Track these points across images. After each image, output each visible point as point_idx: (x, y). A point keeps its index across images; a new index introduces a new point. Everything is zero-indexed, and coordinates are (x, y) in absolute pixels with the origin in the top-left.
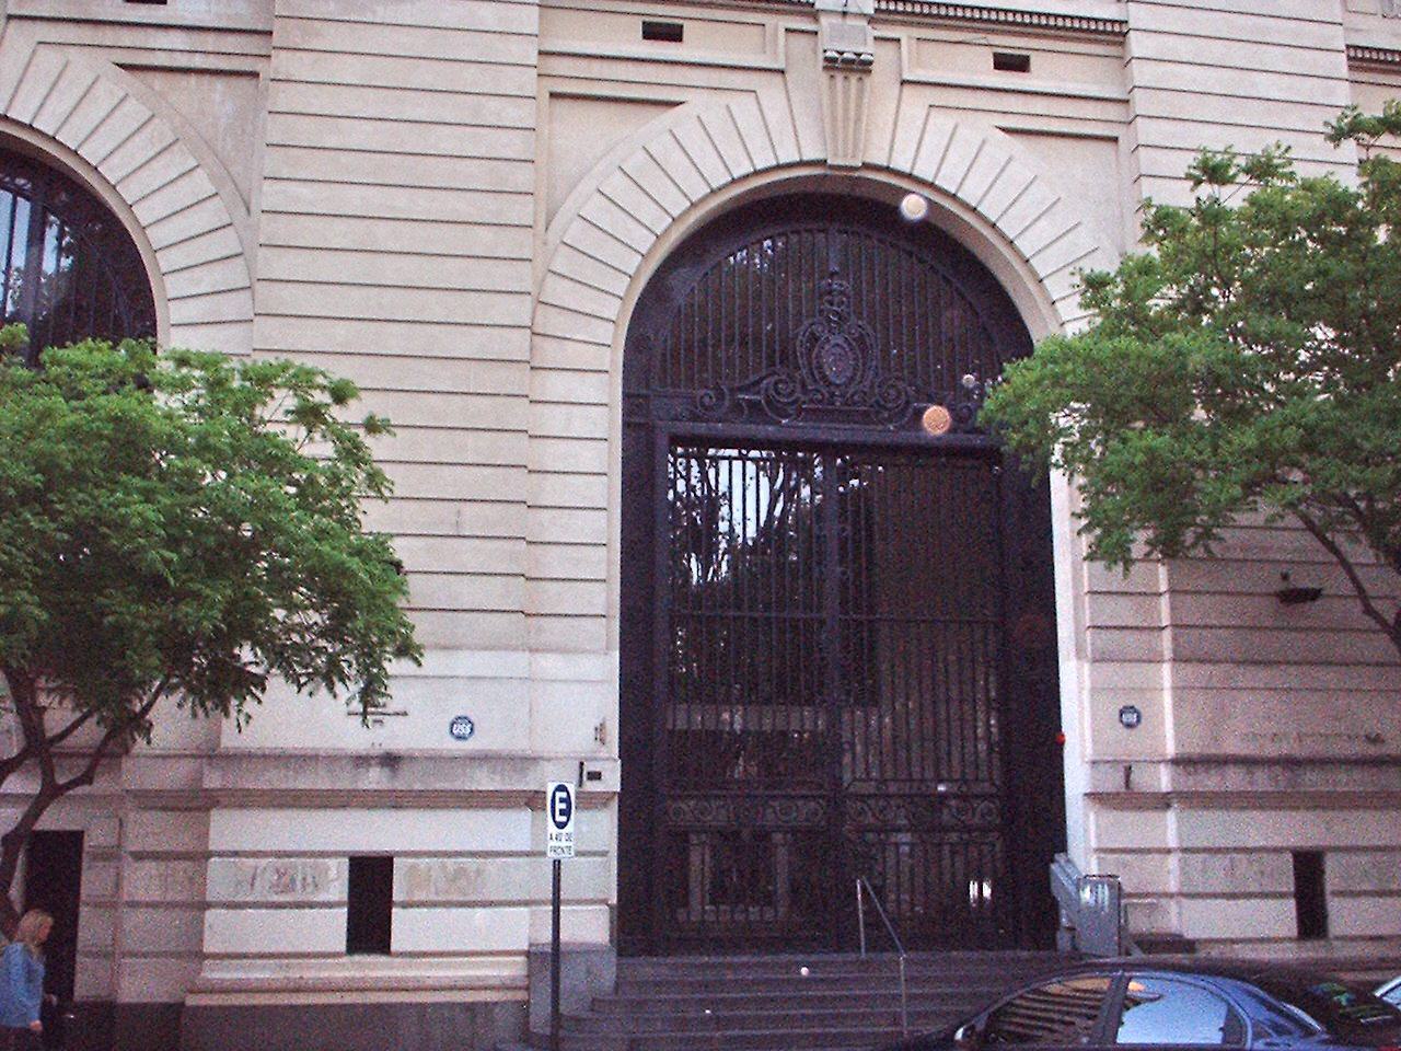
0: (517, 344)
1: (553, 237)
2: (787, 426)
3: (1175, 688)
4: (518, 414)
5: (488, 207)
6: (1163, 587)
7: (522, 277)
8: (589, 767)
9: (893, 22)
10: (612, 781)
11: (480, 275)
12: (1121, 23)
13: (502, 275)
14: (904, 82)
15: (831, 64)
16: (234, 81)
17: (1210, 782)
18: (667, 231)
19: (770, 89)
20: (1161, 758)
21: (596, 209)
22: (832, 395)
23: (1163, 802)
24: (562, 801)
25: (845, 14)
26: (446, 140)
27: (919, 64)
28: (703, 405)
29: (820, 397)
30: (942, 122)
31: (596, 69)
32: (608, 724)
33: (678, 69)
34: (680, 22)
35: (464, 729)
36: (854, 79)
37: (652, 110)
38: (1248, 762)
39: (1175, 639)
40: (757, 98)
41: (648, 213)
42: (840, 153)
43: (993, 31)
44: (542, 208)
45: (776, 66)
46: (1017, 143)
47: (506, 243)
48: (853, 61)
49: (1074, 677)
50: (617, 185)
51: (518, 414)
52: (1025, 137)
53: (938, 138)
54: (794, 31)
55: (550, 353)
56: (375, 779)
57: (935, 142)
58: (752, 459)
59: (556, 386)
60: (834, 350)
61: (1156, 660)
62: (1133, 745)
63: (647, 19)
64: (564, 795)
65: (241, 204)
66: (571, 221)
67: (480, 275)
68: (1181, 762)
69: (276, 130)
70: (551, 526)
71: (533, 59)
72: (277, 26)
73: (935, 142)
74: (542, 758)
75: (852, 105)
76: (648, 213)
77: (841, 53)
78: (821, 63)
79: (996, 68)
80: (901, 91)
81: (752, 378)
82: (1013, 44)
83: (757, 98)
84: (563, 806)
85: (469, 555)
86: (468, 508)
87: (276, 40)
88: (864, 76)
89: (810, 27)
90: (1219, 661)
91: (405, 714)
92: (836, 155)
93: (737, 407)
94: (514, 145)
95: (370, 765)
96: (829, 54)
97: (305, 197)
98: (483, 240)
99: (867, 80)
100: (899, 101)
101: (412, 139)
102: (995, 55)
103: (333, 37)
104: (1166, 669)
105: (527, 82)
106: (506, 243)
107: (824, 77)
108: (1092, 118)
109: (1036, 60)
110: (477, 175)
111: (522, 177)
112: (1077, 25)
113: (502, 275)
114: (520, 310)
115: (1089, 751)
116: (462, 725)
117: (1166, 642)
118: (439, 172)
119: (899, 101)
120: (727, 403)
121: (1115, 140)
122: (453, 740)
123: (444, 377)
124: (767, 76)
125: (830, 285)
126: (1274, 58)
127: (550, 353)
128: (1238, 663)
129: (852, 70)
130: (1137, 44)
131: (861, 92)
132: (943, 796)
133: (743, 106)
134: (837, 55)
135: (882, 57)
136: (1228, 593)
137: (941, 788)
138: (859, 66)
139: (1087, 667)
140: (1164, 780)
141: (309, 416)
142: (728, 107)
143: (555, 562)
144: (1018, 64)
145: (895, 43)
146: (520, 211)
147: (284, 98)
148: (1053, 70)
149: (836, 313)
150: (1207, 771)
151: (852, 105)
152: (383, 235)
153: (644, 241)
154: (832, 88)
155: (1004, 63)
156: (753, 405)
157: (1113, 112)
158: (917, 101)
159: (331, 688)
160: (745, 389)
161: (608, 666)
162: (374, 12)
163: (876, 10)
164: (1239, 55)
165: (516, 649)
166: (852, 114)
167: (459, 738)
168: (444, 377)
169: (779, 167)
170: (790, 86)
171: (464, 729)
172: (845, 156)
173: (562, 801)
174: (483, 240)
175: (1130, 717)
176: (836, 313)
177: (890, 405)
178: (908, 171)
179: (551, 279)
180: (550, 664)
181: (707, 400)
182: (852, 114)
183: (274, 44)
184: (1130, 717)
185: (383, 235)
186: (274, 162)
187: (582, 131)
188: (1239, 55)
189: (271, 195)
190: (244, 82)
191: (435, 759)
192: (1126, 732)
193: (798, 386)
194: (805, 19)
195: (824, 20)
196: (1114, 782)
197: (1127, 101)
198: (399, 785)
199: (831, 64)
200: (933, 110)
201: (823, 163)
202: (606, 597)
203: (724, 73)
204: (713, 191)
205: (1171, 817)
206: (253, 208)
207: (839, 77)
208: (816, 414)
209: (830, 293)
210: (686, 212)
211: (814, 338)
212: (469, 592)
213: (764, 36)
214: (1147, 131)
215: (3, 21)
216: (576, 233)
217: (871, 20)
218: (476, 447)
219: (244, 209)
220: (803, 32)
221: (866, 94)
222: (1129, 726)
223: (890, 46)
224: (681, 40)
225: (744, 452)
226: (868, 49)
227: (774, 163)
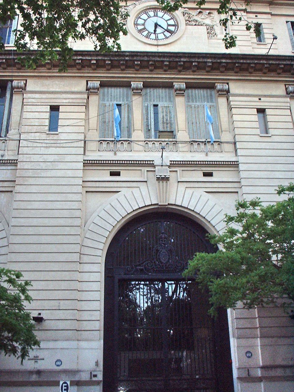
0: (76, 257)
1: (86, 228)
2: (151, 275)
3: (261, 346)
4: (78, 276)
5: (69, 222)
6: (257, 316)
7: (78, 239)
8: (94, 373)
9: (176, 167)
10: (100, 377)
11: (65, 239)
12: (237, 162)
13: (72, 239)
14: (178, 182)
15: (158, 179)
16: (6, 193)
17: (272, 373)
18: (116, 225)
19: (143, 186)
20: (258, 366)
21: (97, 220)
22: (163, 266)
23: (260, 380)
24: (65, 386)
25: (162, 166)
26: (58, 205)
27: (183, 177)
28: (127, 270)
29: (159, 266)
30: (189, 191)
31: (98, 184)
32: (99, 362)
33: (105, 183)
34: (211, 171)
35: (59, 363)
36: (165, 182)
37: (112, 193)
38: (284, 367)
39: (260, 331)
40: (140, 189)
41: (111, 221)
42: (165, 201)
43: (203, 167)
44: (84, 222)
45: (145, 180)
46: (210, 195)
47: (73, 231)
48: (164, 178)
49: (233, 342)
50: (103, 214)
51: (78, 276)
52: (210, 194)
53: (189, 196)
54: (149, 171)
55: (85, 259)
56: (34, 378)
57: (187, 197)
58: (142, 284)
59: (87, 268)
60: (163, 254)
61: (255, 337)
62: (251, 362)
63: (111, 171)
64: (66, 385)
65: (7, 224)
66: (91, 224)
67: (65, 239)
68: (263, 368)
69: (15, 205)
70: (85, 306)
71: (81, 183)
72: (17, 179)
73: (187, 197)
74: (80, 371)
75: (165, 188)
76: (111, 221)
77: (161, 176)
78: (156, 179)
79: (110, 175)
80: (178, 184)
81: (141, 262)
82: (115, 169)
83: (140, 189)
84: (66, 388)
85: (61, 315)
86: (62, 302)
87: (16, 183)
88: (167, 181)
89: (154, 170)
90: (274, 337)
91: (43, 359)
92: (161, 202)
93: (137, 270)
94: (75, 205)
95: (33, 374)
96: (157, 176)
97: (23, 222)
98: (67, 230)
99: (168, 182)
100: (178, 187)
101: (50, 205)
102: (203, 173)
103: (31, 181)
104: (259, 339)
105: (80, 189)
106: (73, 231)
107: (157, 182)
108: (230, 187)
109: (214, 174)
110: (66, 213)
111: (78, 213)
112: (225, 163)
113: (72, 239)
114: (77, 248)
115: (237, 365)
116: (59, 362)
117: (258, 332)
118: (57, 213)
119: (178, 187)
120: (134, 269)
121: (237, 192)
122: (56, 366)
123: (56, 267)
124: (142, 183)
125: (162, 236)
126: (279, 167)
127: (85, 259)
128: (280, 337)
129: (163, 180)
130: (241, 167)
131: (167, 185)
132: (198, 379)
133: (136, 191)
134: (159, 176)
135: (172, 176)
136: (277, 317)
137: (197, 377)
138: (166, 179)
139: (236, 340)
140: (259, 373)
141: (10, 281)
142: (132, 192)
143: (86, 316)
144: (210, 174)
145: (176, 172)
146: (78, 222)
147: (18, 197)
148: (219, 175)
149: (163, 244)
150: (271, 370)
151: (165, 188)
152: (41, 230)
153: (110, 228)
154: (159, 186)
155: (206, 174)
156: (142, 270)
157: (236, 185)
158: (182, 187)
159: (14, 354)
160: (139, 265)
161: (101, 344)
162: (41, 174)
163: (170, 164)
164: (270, 167)
165: (74, 340)
166: (165, 192)
167: (58, 366)
168: (56, 267)
169: (146, 206)
170: (148, 186)
171: (59, 363)
172: (163, 202)
173: (65, 386)
174: (67, 230)
175: (249, 354)
176: (163, 244)
177: (179, 268)
178: (180, 205)
179: (85, 239)
180: (83, 344)
181: (128, 269)
182: (165, 192)
183: (16, 184)
184: (249, 354)
185: (41, 230)
186: (15, 213)
187: (94, 200)
188: (270, 167)
189: (13, 222)
190: (9, 194)
191: (51, 372)
192: (247, 358)
193: (154, 264)
194: (151, 168)
195: (157, 168)
196: (245, 375)
197: (240, 182)
198: (41, 379)
199: (158, 179)
200: (187, 188)
201: (157, 204)
202: (99, 325)
203: (227, 184)
204: (193, 210)
205: (262, 384)
206: (10, 225)
207: (161, 182)
208: (159, 271)
209: (162, 238)
210: (121, 219)
211: (157, 250)
212: (61, 325)
213: (141, 173)
214: (245, 190)
215: (177, 183)
216: (92, 227)
217: (169, 167)
218: (64, 285)
219: (8, 226)
220: (152, 171)
221: (168, 186)
222: (249, 357)
223: (174, 173)
224: (120, 175)
225: (140, 282)
226: (168, 174)
227: (144, 205)
